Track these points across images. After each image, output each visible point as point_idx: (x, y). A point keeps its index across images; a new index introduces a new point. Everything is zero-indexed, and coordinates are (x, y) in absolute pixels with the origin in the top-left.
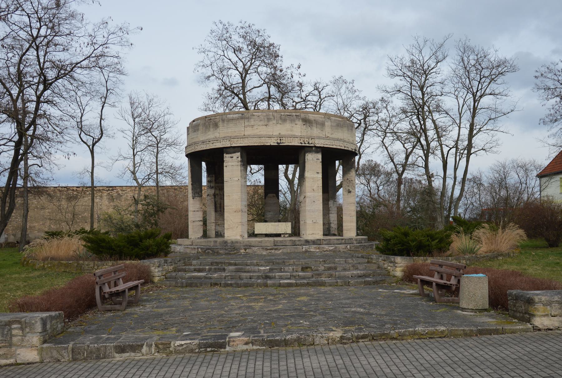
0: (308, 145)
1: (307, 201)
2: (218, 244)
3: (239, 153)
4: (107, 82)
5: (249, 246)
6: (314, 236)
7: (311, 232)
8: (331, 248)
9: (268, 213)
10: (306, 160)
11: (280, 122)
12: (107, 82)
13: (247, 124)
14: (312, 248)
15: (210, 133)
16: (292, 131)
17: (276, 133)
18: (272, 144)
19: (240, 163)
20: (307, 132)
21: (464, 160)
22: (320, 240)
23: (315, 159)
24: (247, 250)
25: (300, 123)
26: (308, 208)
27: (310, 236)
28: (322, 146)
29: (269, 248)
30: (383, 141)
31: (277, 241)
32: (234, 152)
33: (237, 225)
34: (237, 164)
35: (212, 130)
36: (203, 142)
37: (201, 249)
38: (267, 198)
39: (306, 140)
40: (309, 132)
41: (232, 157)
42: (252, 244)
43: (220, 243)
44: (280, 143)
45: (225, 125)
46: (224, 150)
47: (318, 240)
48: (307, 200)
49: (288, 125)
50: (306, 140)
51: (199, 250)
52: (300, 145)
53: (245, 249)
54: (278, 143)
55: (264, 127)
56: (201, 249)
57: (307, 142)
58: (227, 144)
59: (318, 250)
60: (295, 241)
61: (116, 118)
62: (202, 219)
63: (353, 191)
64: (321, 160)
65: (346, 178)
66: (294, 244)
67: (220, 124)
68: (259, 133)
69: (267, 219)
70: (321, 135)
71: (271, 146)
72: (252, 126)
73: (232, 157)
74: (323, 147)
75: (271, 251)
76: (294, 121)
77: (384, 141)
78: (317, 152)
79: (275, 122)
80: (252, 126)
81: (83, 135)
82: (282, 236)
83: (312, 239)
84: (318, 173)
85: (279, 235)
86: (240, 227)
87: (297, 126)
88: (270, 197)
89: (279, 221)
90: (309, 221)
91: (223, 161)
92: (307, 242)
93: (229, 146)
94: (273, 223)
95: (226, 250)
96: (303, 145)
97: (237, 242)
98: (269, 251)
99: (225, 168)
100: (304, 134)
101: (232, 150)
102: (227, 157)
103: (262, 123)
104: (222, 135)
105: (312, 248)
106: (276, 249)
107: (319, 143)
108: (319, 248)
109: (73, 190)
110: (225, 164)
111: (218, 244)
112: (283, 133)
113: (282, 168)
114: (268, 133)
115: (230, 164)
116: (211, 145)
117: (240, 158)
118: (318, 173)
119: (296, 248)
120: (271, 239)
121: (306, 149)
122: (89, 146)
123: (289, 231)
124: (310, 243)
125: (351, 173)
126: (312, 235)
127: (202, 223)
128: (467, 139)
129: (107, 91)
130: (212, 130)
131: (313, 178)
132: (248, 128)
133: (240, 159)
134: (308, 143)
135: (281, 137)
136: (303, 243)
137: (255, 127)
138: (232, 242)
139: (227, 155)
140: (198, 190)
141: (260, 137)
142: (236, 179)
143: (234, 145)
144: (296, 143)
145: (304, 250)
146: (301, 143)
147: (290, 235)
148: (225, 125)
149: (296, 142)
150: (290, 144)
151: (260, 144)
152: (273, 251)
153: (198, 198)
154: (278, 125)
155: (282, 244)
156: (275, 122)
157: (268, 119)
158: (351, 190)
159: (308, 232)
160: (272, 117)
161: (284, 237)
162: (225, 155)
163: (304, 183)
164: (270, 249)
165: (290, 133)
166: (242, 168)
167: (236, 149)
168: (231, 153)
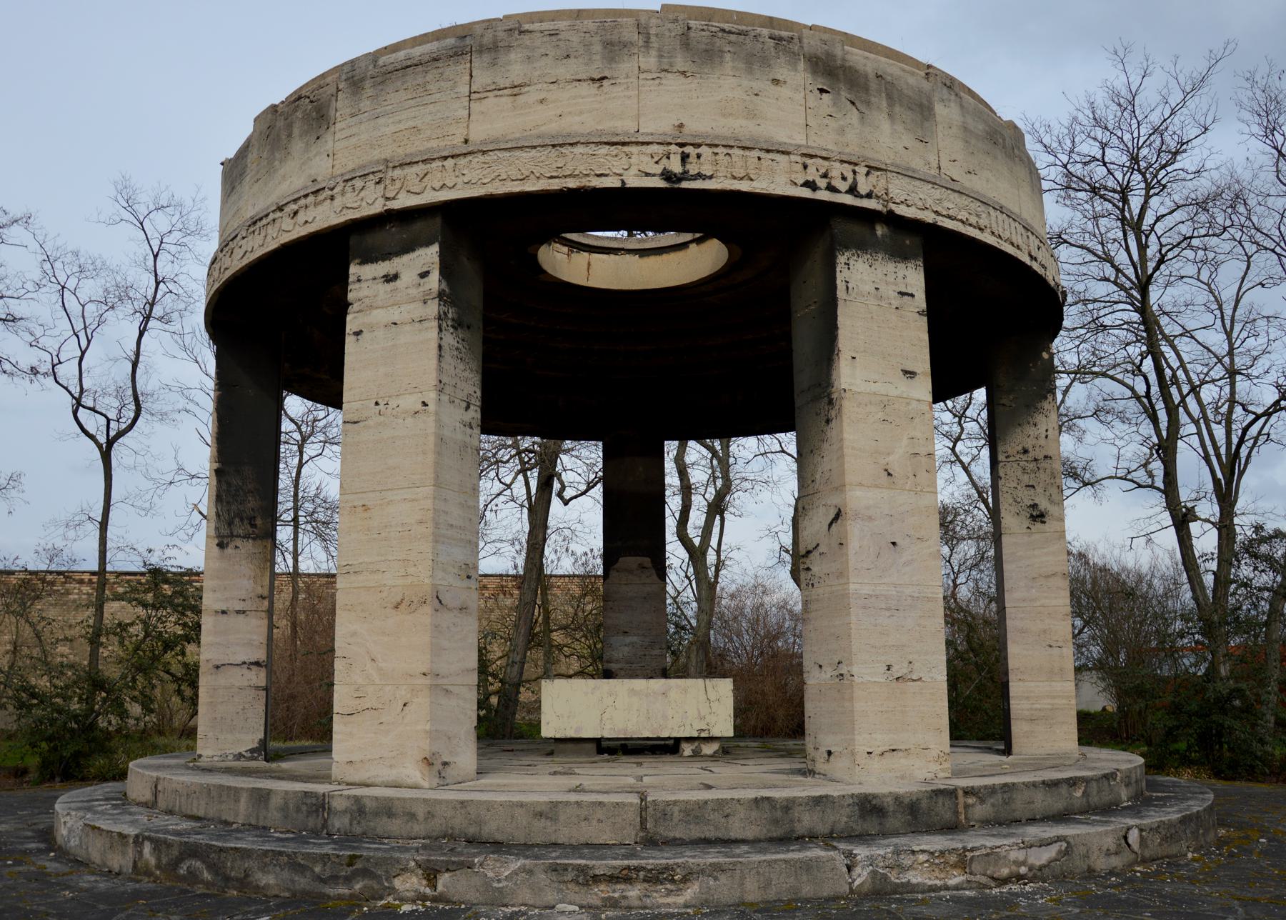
0: (848, 200)
1: (854, 544)
2: (273, 816)
3: (435, 248)
4: (156, 257)
5: (469, 842)
6: (899, 762)
7: (881, 741)
8: (1042, 857)
9: (617, 640)
10: (841, 293)
11: (680, 63)
12: (156, 257)
13: (483, 78)
14: (921, 863)
15: (291, 166)
16: (751, 114)
17: (658, 124)
18: (634, 182)
19: (433, 308)
20: (841, 131)
22: (951, 793)
23: (890, 292)
24: (444, 880)
25: (798, 78)
26: (858, 585)
27: (876, 764)
28: (929, 217)
29: (602, 866)
30: (953, 449)
32: (408, 248)
34: (418, 310)
35: (297, 146)
37: (158, 845)
38: (613, 574)
40: (851, 136)
41: (391, 278)
42: (492, 828)
43: (284, 809)
44: (684, 176)
45: (365, 104)
46: (353, 240)
47: (938, 793)
48: (855, 532)
49: (729, 82)
50: (836, 170)
51: (147, 849)
52: (806, 193)
53: (431, 875)
54: (667, 175)
55: (587, 89)
56: (158, 845)
57: (843, 186)
59: (956, 879)
60: (788, 806)
61: (166, 354)
62: (261, 655)
63: (1052, 509)
64: (921, 301)
65: (1011, 446)
66: (783, 830)
68: (553, 127)
69: (613, 666)
70: (917, 164)
72: (517, 89)
73: (391, 278)
74: (934, 227)
75: (616, 891)
76: (765, 62)
77: (957, 449)
78: (900, 255)
79: (650, 61)
80: (517, 89)
81: (82, 413)
82: (687, 749)
83: (902, 788)
84: (910, 374)
85: (667, 748)
86: (421, 703)
87: (784, 91)
88: (630, 571)
89: (665, 674)
90: (866, 671)
91: (343, 307)
92: (872, 814)
94: (639, 684)
95: (296, 866)
97: (387, 809)
98: (601, 892)
99: (349, 341)
100: (824, 140)
101: (394, 233)
102: (364, 281)
104: (348, 161)
105: (921, 863)
106: (655, 877)
107: (915, 202)
108: (963, 863)
109: (81, 582)
110: (352, 323)
111: (273, 816)
112: (698, 125)
113: (671, 447)
114: (608, 125)
115: (380, 316)
117: (435, 276)
118: (910, 374)
119: (808, 866)
120: (625, 773)
121: (840, 227)
122: (99, 446)
123: (724, 726)
124: (893, 822)
125: (1039, 418)
126: (890, 760)
129: (158, 284)
131: (885, 403)
132: (491, 101)
133: (434, 281)
134: (853, 190)
135: (686, 146)
136: (842, 818)
137: (532, 95)
138: (359, 809)
140: (252, 503)
142: (412, 402)
143: (405, 201)
145: (861, 876)
146: (811, 185)
150: (744, 186)
151: (555, 185)
152: (634, 892)
153: (247, 547)
154: (672, 81)
155: (696, 832)
156: (650, 61)
157: (608, 44)
158: (1044, 504)
159: (863, 742)
161: (696, 754)
162: (354, 269)
163: (832, 432)
164: (613, 879)
165: (740, 127)
166: (450, 339)
167: (418, 226)
168: (386, 256)
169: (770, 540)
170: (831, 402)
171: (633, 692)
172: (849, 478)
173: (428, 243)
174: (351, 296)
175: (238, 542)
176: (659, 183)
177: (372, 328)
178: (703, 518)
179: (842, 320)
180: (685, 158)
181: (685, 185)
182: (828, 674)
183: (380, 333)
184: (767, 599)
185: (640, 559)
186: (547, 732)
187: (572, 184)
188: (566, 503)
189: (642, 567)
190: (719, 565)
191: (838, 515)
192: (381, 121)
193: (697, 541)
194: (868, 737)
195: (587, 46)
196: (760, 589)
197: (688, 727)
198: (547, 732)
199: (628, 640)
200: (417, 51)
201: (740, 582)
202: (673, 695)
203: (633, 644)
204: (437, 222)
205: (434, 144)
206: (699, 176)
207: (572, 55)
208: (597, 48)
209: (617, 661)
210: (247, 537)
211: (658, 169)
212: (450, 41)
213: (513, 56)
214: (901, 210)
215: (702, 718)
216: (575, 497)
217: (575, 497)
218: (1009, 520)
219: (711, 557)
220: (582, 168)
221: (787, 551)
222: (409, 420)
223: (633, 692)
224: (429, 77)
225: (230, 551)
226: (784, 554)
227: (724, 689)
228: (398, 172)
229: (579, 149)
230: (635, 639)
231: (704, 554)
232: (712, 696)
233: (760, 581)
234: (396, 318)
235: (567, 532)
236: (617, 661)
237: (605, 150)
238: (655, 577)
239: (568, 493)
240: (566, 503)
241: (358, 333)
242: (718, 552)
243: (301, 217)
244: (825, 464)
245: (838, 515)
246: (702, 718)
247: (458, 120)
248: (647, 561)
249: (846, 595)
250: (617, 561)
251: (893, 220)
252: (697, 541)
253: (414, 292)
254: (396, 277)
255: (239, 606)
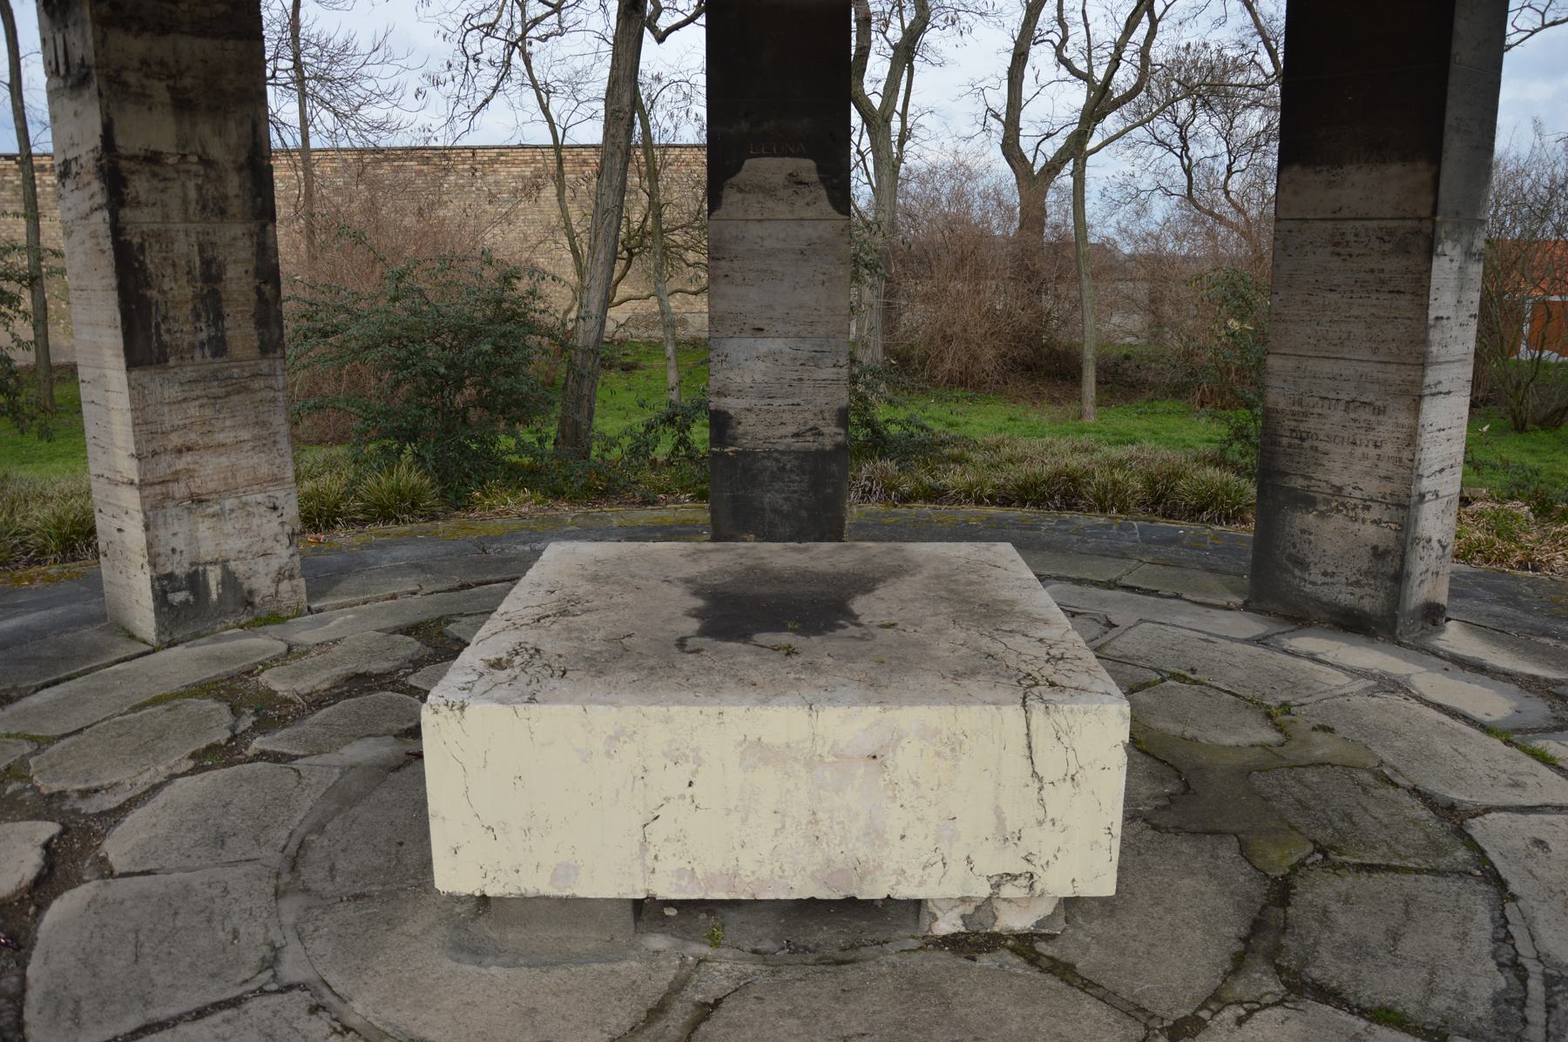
38: (731, 197)
88: (769, 192)
169: (971, 98)
171: (757, 751)
178: (887, 65)
184: (971, 184)
185: (790, 164)
186: (454, 875)
188: (661, 38)
189: (796, 181)
190: (905, 135)
193: (876, 101)
196: (962, 172)
197: (957, 869)
198: (454, 875)
199: (764, 345)
201: (931, 158)
202: (908, 760)
203: (774, 356)
207: (879, 760)
209: (740, 393)
215: (1008, 838)
216: (677, 27)
217: (677, 27)
219: (896, 124)
221: (997, 116)
223: (757, 751)
226: (991, 120)
230: (778, 344)
231: (887, 121)
232: (1051, 761)
233: (961, 158)
235: (686, 87)
236: (740, 393)
238: (825, 205)
239: (664, 22)
240: (661, 38)
242: (903, 116)
246: (1008, 838)
248: (806, 167)
250: (738, 168)
252: (876, 101)
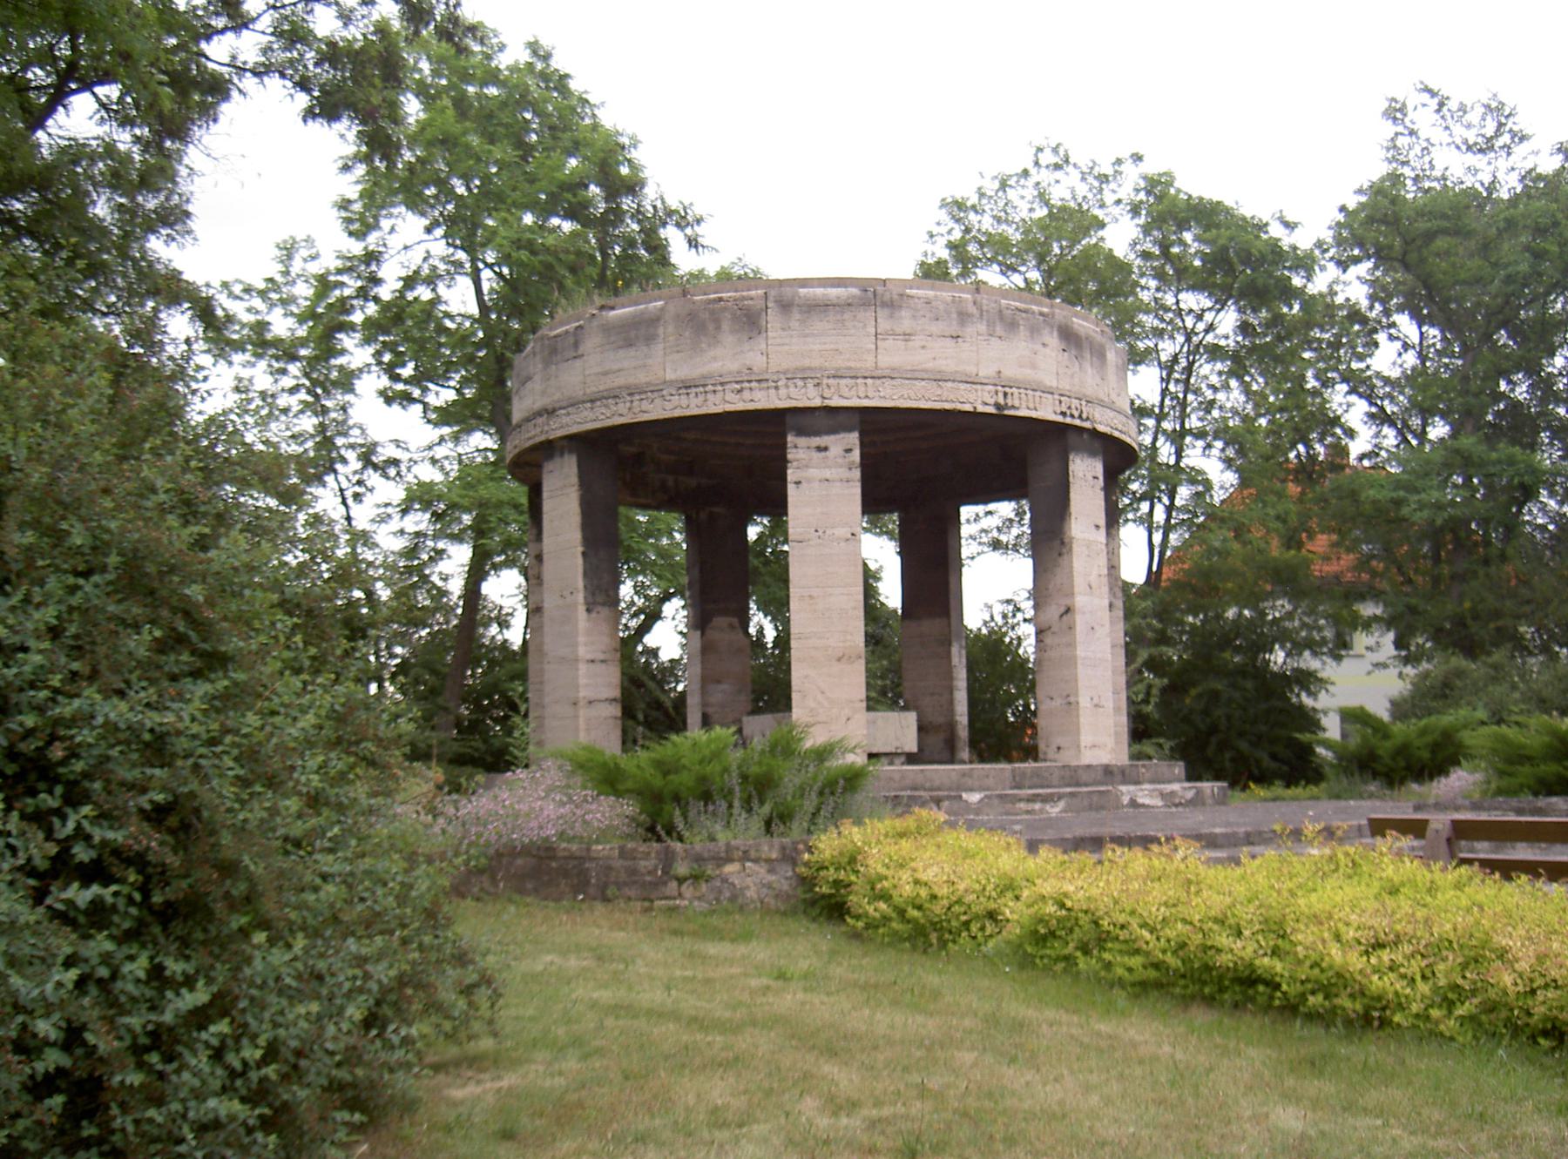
0: (1077, 422)
11: (999, 330)
13: (884, 325)
16: (1033, 366)
18: (981, 409)
20: (1072, 376)
21: (1154, 568)
25: (1053, 340)
31: (1023, 774)
32: (833, 431)
33: (847, 712)
34: (843, 473)
35: (728, 339)
36: (686, 386)
39: (1075, 403)
44: (1006, 407)
45: (795, 324)
46: (789, 419)
52: (1060, 419)
54: (997, 406)
55: (950, 343)
57: (1076, 414)
58: (808, 397)
67: (773, 318)
68: (930, 365)
71: (975, 415)
72: (907, 336)
75: (1030, 806)
80: (907, 336)
87: (1047, 351)
90: (1084, 701)
93: (817, 402)
96: (1068, 420)
99: (791, 488)
102: (799, 450)
103: (936, 328)
110: (792, 475)
112: (1010, 372)
114: (961, 368)
115: (813, 472)
116: (730, 396)
123: (911, 746)
127: (616, 710)
128: (963, 542)
130: (728, 339)
132: (890, 342)
133: (856, 455)
135: (1004, 385)
137: (917, 341)
139: (803, 441)
141: (939, 379)
144: (1047, 411)
146: (1063, 414)
147: (911, 759)
148: (795, 324)
149: (1050, 409)
150: (1034, 414)
151: (938, 406)
152: (1037, 806)
160: (972, 310)
162: (790, 438)
163: (1064, 560)
168: (817, 433)
170: (1063, 543)
172: (1076, 590)
173: (850, 430)
174: (789, 457)
175: (599, 608)
176: (991, 410)
177: (809, 481)
179: (1072, 495)
180: (1005, 394)
181: (1006, 412)
182: (1058, 702)
183: (816, 485)
187: (948, 406)
191: (1068, 610)
192: (809, 340)
194: (1086, 739)
195: (948, 313)
200: (833, 292)
204: (856, 418)
205: (852, 364)
206: (1013, 407)
208: (954, 316)
210: (603, 604)
211: (992, 401)
212: (854, 291)
213: (903, 313)
214: (1101, 428)
218: (350, 501)
220: (952, 397)
222: (843, 544)
224: (846, 316)
225: (594, 615)
227: (911, 718)
228: (831, 381)
229: (950, 384)
234: (828, 476)
237: (963, 386)
241: (798, 483)
243: (746, 395)
244: (1058, 579)
245: (1068, 610)
247: (869, 351)
248: (735, 621)
249: (1075, 657)
251: (1094, 433)
253: (840, 460)
254: (826, 449)
255: (602, 657)
